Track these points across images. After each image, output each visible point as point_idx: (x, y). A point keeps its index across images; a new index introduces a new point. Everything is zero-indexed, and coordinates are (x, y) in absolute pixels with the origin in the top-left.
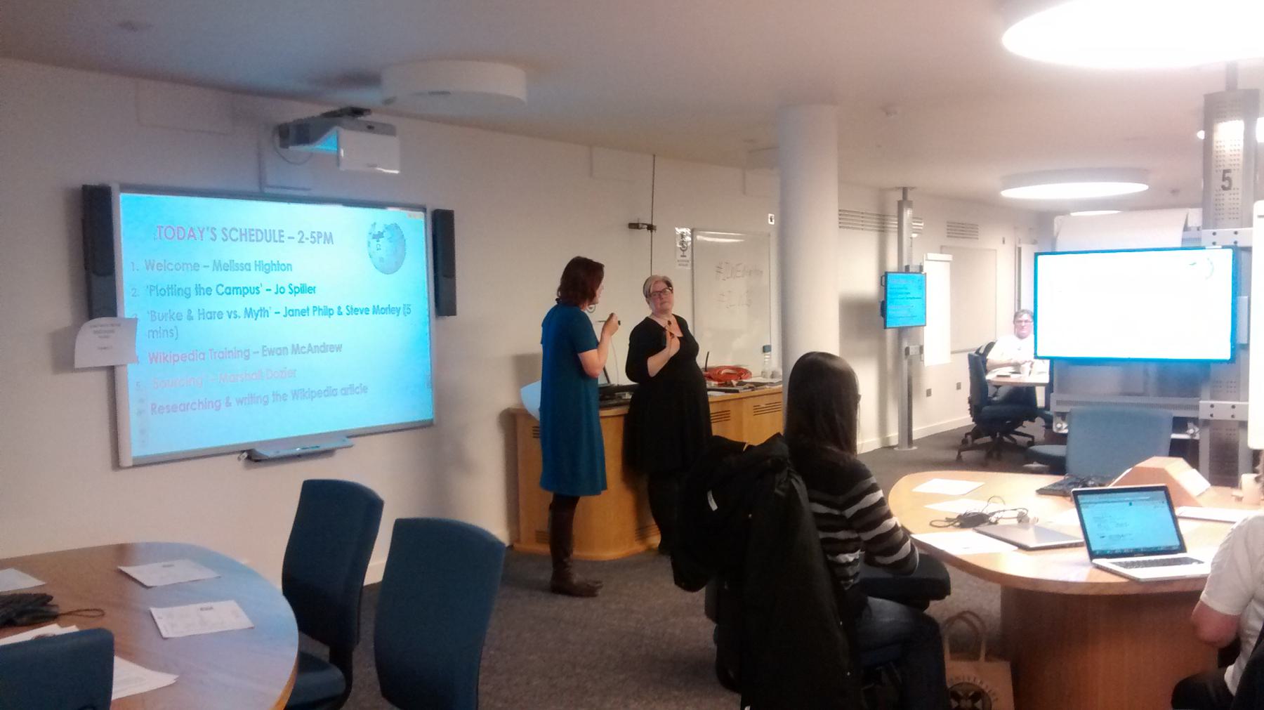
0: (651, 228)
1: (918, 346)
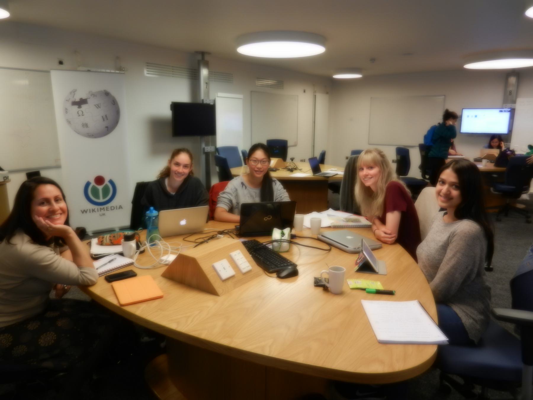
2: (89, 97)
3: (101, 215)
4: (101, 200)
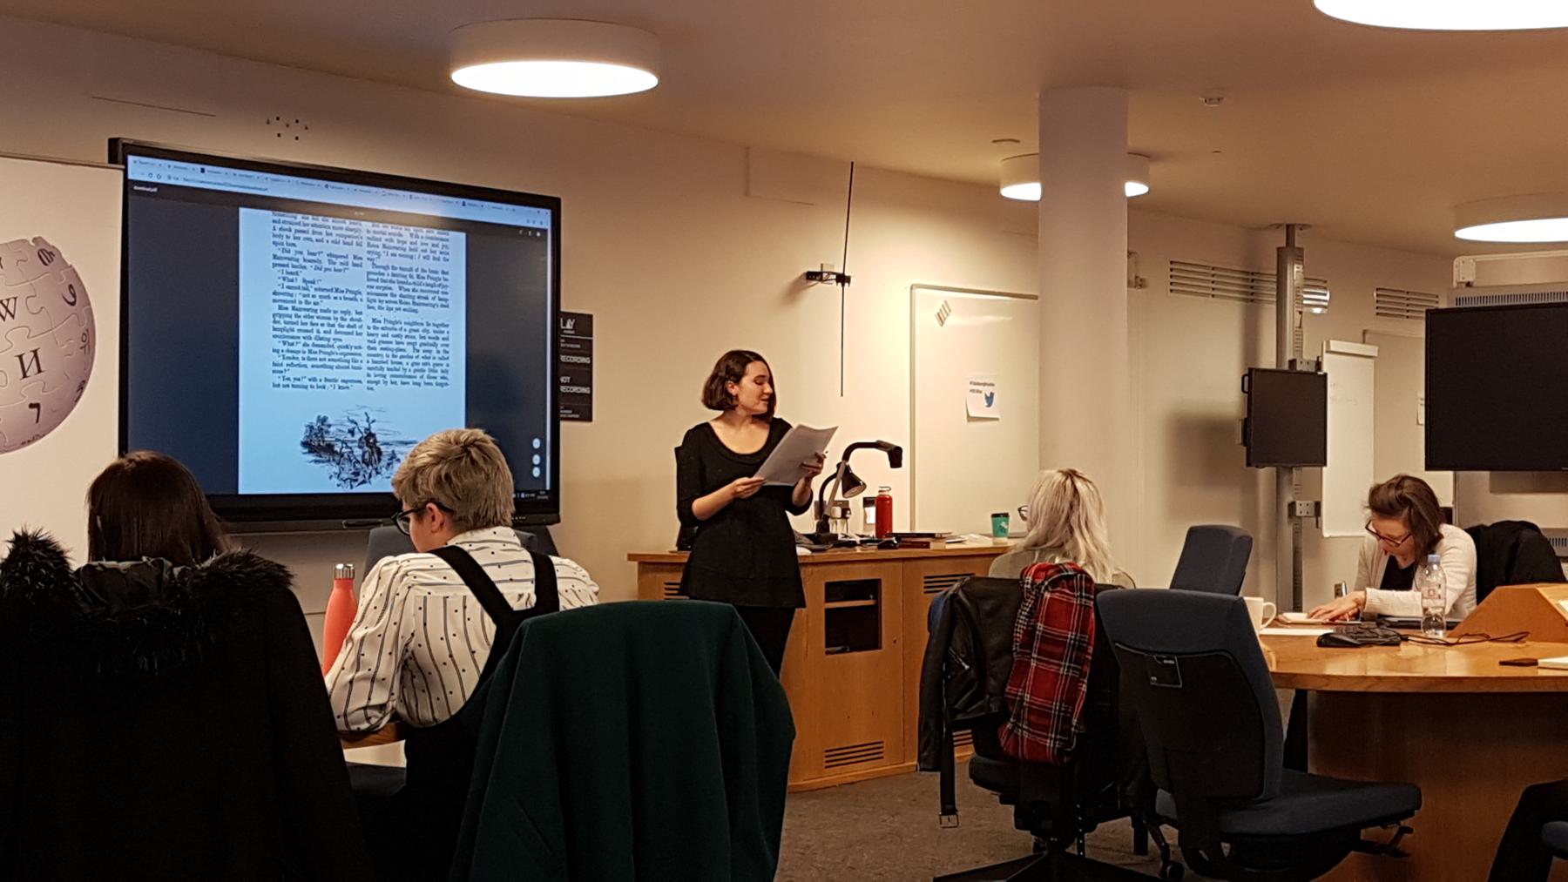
0: (842, 279)
1: (1311, 502)
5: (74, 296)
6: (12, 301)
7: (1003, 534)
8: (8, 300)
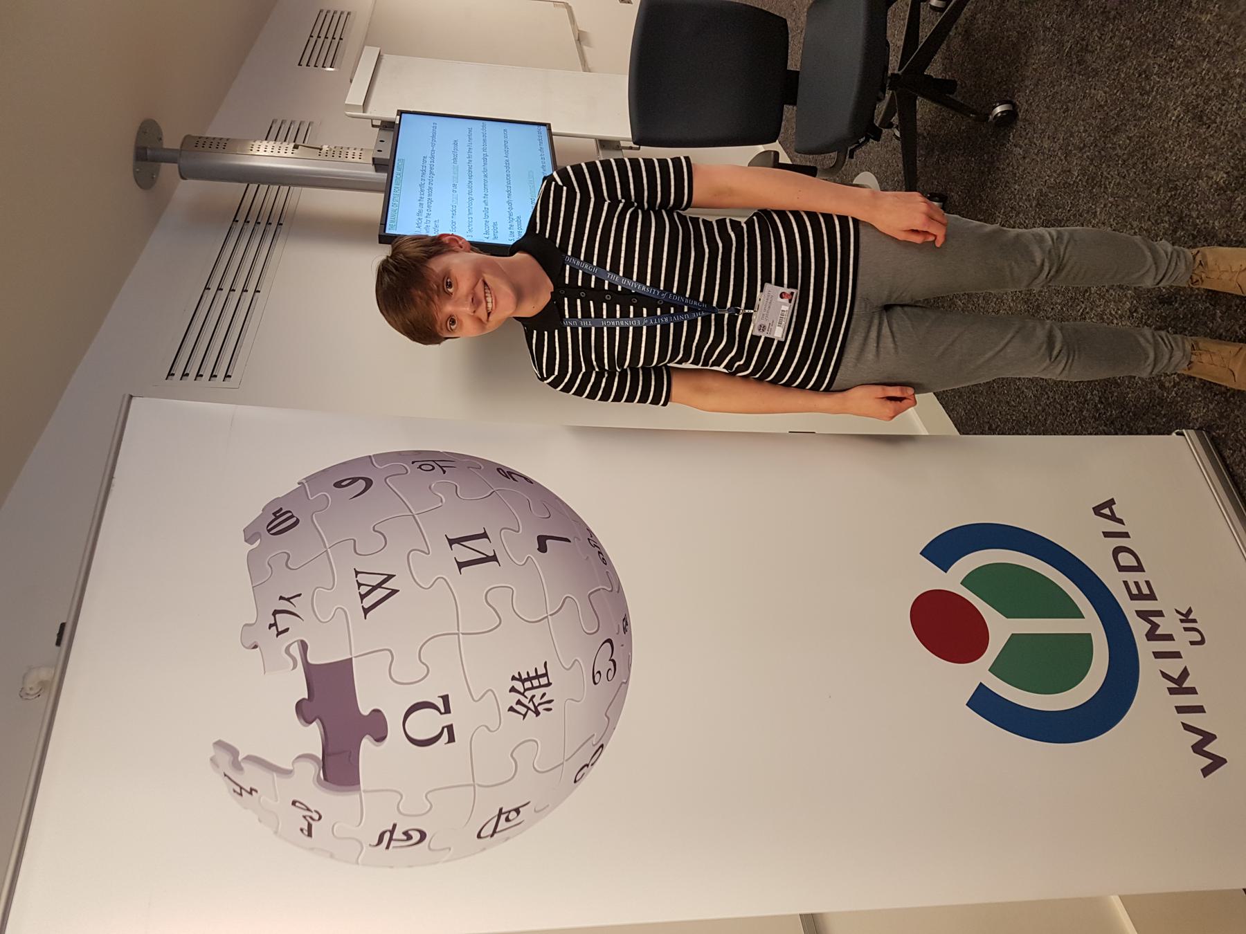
2: (295, 651)
3: (1196, 637)
4: (1090, 623)
5: (354, 480)
6: (361, 578)
7: (476, 305)
8: (360, 585)
